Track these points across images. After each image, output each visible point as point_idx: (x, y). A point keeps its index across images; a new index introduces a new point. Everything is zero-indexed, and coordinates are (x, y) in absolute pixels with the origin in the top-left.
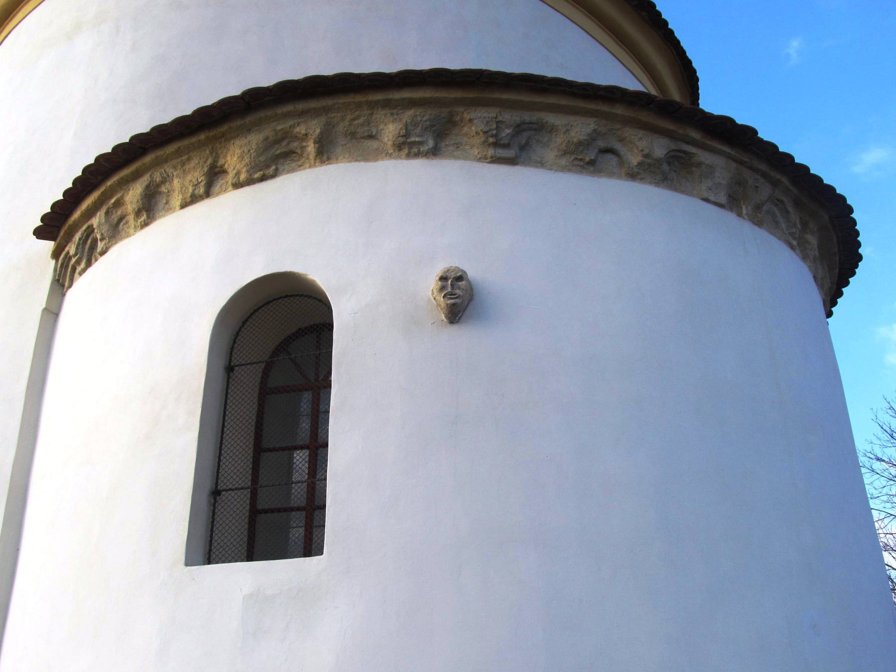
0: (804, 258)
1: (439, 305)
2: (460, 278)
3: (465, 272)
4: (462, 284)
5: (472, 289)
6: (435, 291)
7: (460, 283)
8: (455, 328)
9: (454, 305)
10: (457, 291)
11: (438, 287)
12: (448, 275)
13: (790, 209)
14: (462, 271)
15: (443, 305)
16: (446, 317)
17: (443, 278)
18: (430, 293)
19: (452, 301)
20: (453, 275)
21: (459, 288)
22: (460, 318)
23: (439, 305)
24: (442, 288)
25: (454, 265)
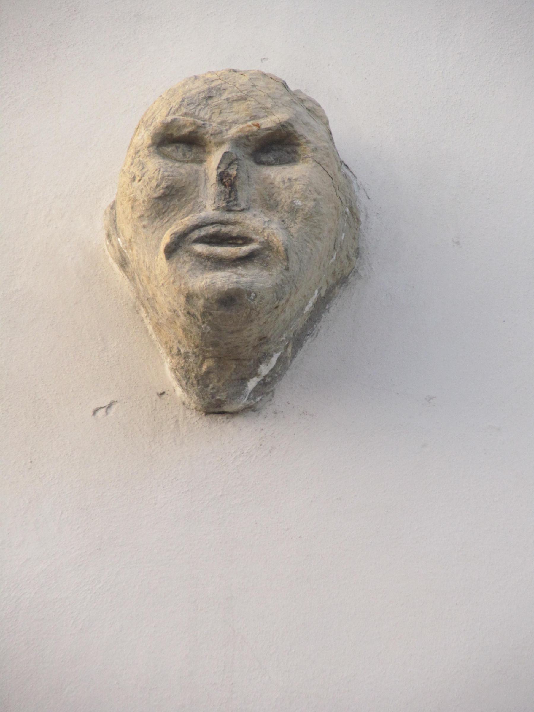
0: (285, 122)
1: (146, 301)
2: (276, 145)
3: (315, 111)
4: (287, 177)
5: (351, 215)
6: (124, 211)
7: (277, 174)
8: (236, 437)
9: (229, 300)
10: (257, 223)
11: (143, 192)
12: (211, 119)
13: (268, 132)
14: (299, 99)
15: (168, 300)
16: (185, 375)
17: (178, 140)
18: (100, 224)
19: (223, 279)
20: (234, 122)
21: (269, 203)
22: (266, 387)
23: (146, 301)
24: (169, 197)
25: (249, 63)
